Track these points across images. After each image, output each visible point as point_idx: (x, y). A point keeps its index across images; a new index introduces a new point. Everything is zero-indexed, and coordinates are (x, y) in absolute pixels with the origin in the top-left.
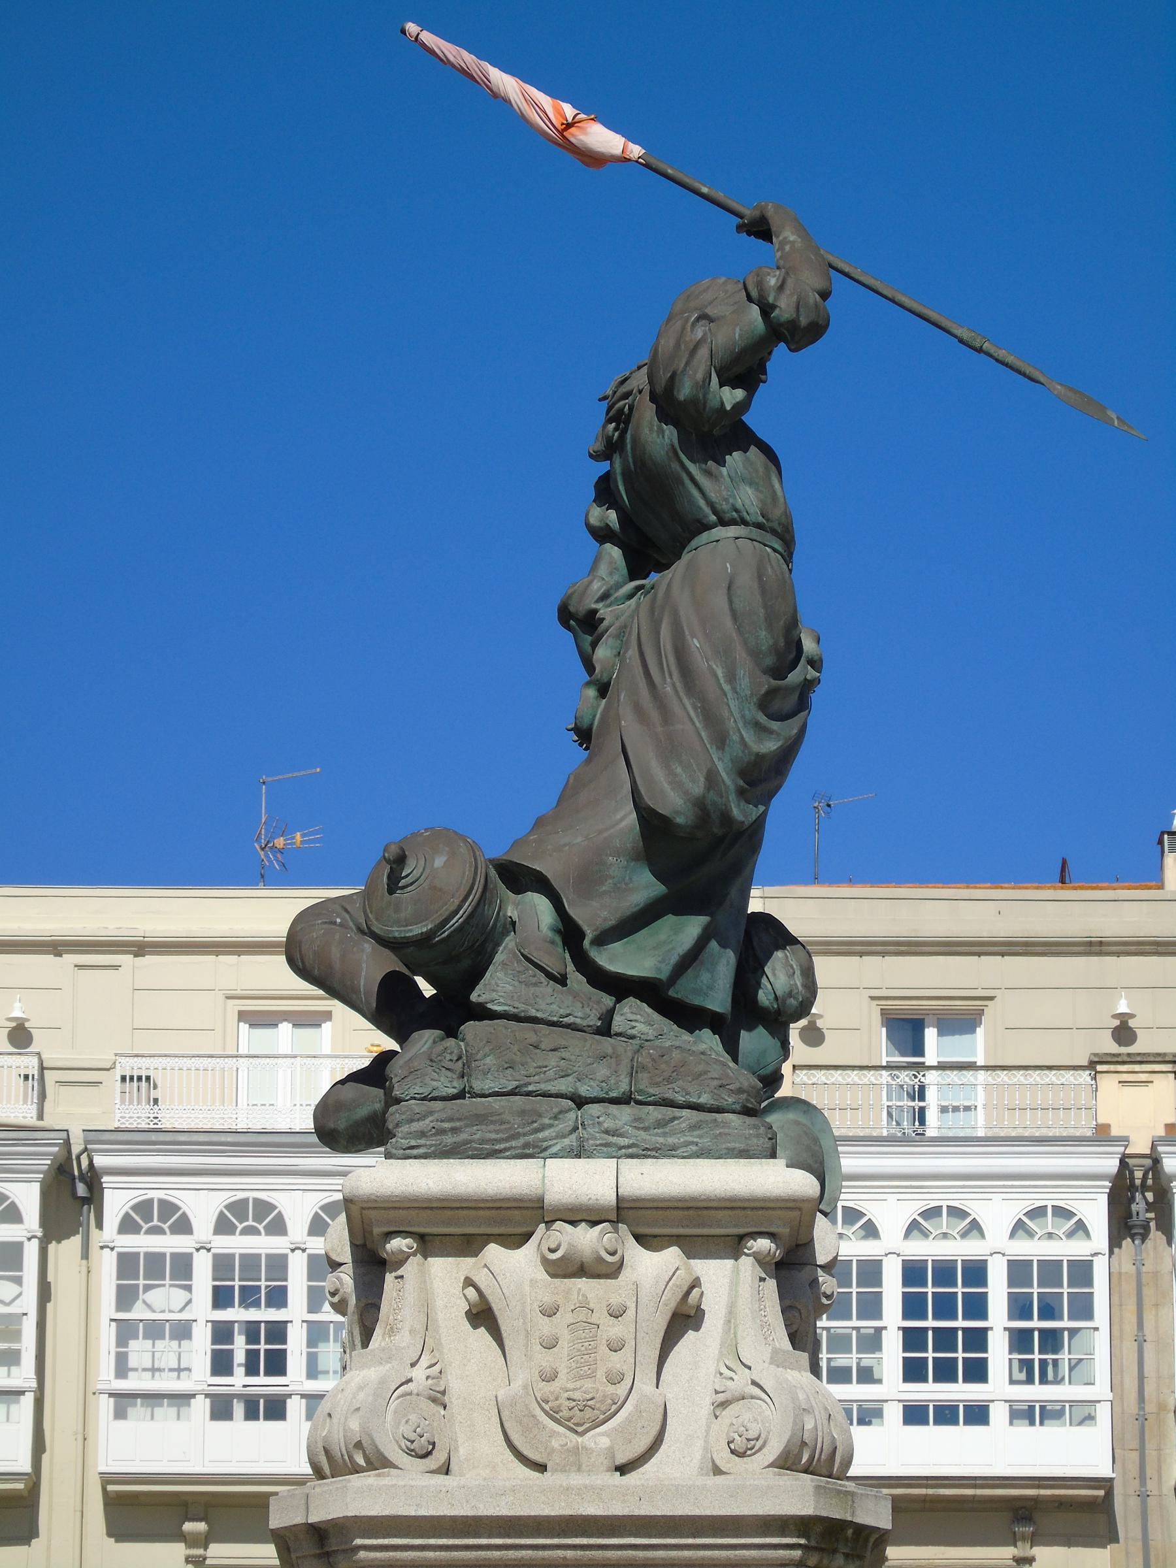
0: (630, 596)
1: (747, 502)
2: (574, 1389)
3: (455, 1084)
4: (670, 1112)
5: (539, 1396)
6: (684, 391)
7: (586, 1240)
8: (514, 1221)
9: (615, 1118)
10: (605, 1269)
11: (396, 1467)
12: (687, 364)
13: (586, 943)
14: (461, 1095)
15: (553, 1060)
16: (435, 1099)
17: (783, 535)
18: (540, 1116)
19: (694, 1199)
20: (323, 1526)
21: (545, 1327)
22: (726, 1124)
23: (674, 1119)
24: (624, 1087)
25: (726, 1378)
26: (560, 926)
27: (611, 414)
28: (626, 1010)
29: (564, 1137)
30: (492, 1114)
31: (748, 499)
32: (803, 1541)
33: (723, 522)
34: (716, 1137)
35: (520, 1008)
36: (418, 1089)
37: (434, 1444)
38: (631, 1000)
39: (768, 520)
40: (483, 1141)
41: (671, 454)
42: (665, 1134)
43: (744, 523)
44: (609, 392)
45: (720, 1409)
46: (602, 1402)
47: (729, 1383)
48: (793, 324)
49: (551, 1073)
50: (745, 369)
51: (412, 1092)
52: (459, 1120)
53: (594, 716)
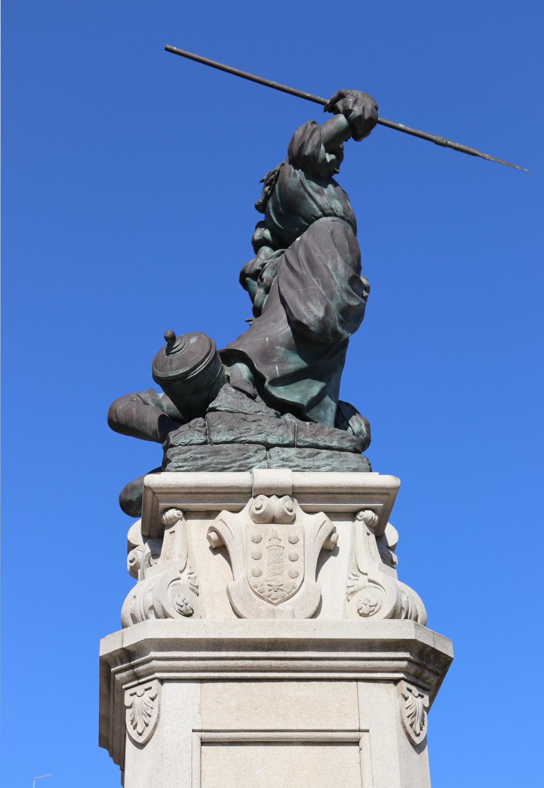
0: (278, 256)
1: (337, 206)
3: (202, 437)
4: (316, 450)
5: (251, 584)
6: (308, 150)
7: (277, 505)
9: (287, 452)
12: (310, 137)
13: (266, 384)
14: (205, 443)
15: (253, 426)
16: (192, 445)
18: (248, 451)
19: (333, 488)
20: (132, 649)
23: (319, 453)
24: (291, 438)
25: (353, 580)
26: (253, 378)
29: (260, 461)
30: (222, 451)
31: (337, 205)
32: (407, 655)
33: (325, 215)
34: (341, 462)
36: (182, 440)
37: (193, 610)
40: (218, 463)
41: (300, 185)
42: (314, 461)
43: (335, 215)
46: (287, 587)
47: (356, 582)
48: (361, 117)
51: (179, 442)
52: (205, 453)
53: (263, 301)
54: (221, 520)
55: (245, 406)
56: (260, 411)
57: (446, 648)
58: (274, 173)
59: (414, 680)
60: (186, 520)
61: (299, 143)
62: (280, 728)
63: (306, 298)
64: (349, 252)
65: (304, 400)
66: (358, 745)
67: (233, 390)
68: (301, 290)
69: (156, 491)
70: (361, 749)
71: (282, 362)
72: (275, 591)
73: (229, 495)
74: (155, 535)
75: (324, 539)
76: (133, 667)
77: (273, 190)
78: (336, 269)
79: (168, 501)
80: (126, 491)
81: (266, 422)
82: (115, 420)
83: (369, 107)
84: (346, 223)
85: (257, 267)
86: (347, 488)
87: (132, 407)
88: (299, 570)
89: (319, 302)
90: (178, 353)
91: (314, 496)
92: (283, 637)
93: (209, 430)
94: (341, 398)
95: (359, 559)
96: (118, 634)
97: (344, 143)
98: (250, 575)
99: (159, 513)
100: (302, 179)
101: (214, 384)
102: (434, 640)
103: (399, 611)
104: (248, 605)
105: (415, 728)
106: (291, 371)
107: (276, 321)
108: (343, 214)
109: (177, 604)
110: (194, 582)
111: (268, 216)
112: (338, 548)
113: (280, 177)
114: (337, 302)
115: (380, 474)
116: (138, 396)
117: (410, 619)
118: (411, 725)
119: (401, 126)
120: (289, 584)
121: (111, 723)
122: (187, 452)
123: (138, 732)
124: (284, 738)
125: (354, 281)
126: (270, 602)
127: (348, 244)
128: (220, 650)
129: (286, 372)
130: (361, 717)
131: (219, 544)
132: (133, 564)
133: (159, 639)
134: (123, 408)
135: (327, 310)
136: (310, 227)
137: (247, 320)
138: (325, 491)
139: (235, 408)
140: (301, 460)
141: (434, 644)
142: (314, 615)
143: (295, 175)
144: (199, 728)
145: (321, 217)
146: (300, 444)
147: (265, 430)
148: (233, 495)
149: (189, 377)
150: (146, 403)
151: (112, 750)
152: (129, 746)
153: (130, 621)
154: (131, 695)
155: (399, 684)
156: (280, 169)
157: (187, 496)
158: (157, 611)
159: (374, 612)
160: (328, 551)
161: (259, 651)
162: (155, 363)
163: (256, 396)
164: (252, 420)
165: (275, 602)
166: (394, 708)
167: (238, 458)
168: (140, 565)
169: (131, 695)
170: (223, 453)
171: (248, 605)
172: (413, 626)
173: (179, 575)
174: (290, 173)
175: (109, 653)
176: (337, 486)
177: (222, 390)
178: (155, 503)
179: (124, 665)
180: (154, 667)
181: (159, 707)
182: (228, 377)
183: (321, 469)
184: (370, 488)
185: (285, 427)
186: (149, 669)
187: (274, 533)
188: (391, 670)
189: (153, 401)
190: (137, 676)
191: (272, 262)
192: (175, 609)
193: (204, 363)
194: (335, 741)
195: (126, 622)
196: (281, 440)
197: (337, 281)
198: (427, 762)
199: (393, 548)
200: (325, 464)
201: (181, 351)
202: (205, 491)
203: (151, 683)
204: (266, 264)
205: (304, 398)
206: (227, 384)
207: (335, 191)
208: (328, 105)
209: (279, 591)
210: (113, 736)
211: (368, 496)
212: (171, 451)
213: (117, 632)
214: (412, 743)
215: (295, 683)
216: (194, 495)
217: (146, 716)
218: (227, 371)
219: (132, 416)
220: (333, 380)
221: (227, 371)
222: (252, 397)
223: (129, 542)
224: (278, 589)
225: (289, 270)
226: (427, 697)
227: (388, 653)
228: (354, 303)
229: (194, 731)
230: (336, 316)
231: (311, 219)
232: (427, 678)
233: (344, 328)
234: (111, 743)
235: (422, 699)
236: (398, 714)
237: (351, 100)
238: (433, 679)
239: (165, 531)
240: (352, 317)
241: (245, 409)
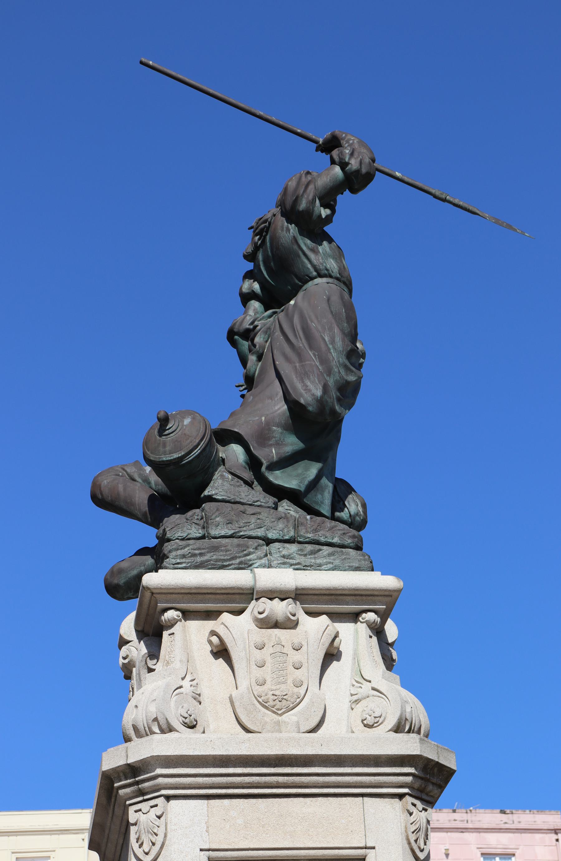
0: (270, 316)
3: (200, 531)
4: (317, 547)
5: (255, 693)
6: (303, 205)
7: (280, 608)
8: (238, 599)
10: (290, 624)
11: (178, 731)
13: (263, 469)
14: (203, 537)
15: (253, 519)
16: (189, 539)
17: (346, 283)
18: (248, 547)
19: (336, 589)
21: (258, 655)
22: (348, 554)
23: (320, 550)
24: (292, 533)
25: (357, 687)
26: (249, 461)
27: (257, 231)
28: (284, 504)
29: (261, 558)
30: (221, 546)
31: (332, 265)
32: (412, 770)
33: (320, 276)
35: (232, 497)
36: (180, 534)
37: (196, 721)
38: (286, 501)
39: (342, 276)
40: (217, 561)
41: (293, 241)
42: (315, 558)
43: (331, 276)
45: (355, 704)
46: (292, 697)
47: (359, 689)
48: (358, 172)
50: (328, 198)
52: (203, 549)
53: (256, 370)
55: (243, 495)
57: (449, 761)
58: (265, 221)
59: (418, 794)
62: (287, 846)
63: (303, 375)
65: (301, 485)
67: (230, 477)
68: (297, 365)
69: (154, 591)
72: (280, 701)
74: (152, 632)
75: (327, 645)
76: (138, 783)
77: (264, 242)
78: (333, 342)
79: (167, 602)
82: (100, 496)
83: (367, 160)
86: (350, 590)
87: (118, 483)
88: (303, 679)
89: (317, 380)
90: (171, 435)
91: (316, 597)
92: (290, 753)
93: (207, 523)
94: (338, 475)
95: (361, 664)
98: (254, 684)
99: (157, 612)
100: (295, 234)
101: (209, 468)
104: (252, 716)
105: (420, 844)
109: (181, 716)
110: (196, 690)
111: (257, 266)
112: (341, 652)
113: (272, 229)
114: (335, 379)
115: (382, 574)
116: (124, 469)
119: (398, 174)
120: (293, 694)
121: (107, 831)
122: (185, 547)
127: (345, 312)
128: (226, 766)
129: (283, 456)
130: (368, 834)
132: (126, 661)
133: (165, 756)
135: (325, 388)
136: (304, 288)
137: (237, 385)
138: (327, 592)
139: (232, 497)
140: (303, 557)
143: (288, 230)
144: (206, 847)
145: (315, 278)
146: (300, 540)
148: (235, 596)
149: (184, 462)
150: (134, 480)
151: (105, 854)
153: (132, 733)
154: (136, 811)
157: (186, 597)
158: (161, 724)
159: (378, 724)
160: (331, 655)
161: (266, 767)
162: (146, 443)
163: (253, 483)
164: (251, 513)
165: (280, 712)
166: (399, 824)
167: (237, 555)
169: (136, 811)
170: (223, 548)
171: (252, 716)
175: (113, 768)
176: (340, 588)
178: (153, 603)
179: (129, 781)
180: (160, 784)
182: (223, 460)
183: (323, 567)
184: (373, 590)
186: (155, 786)
189: (140, 475)
190: (142, 793)
192: (179, 721)
193: (199, 447)
195: (128, 733)
196: (281, 536)
199: (392, 645)
200: (326, 562)
201: (175, 433)
202: (206, 591)
203: (156, 800)
204: (257, 326)
205: (301, 482)
206: (222, 466)
207: (330, 248)
208: (320, 145)
209: (284, 701)
215: (301, 799)
217: (152, 835)
220: (330, 459)
222: (249, 484)
223: (121, 637)
224: (283, 699)
225: (284, 340)
227: (394, 768)
228: (352, 378)
229: (201, 850)
230: (334, 393)
231: (306, 279)
233: (341, 406)
235: (426, 813)
236: (403, 830)
237: (347, 151)
240: (348, 392)
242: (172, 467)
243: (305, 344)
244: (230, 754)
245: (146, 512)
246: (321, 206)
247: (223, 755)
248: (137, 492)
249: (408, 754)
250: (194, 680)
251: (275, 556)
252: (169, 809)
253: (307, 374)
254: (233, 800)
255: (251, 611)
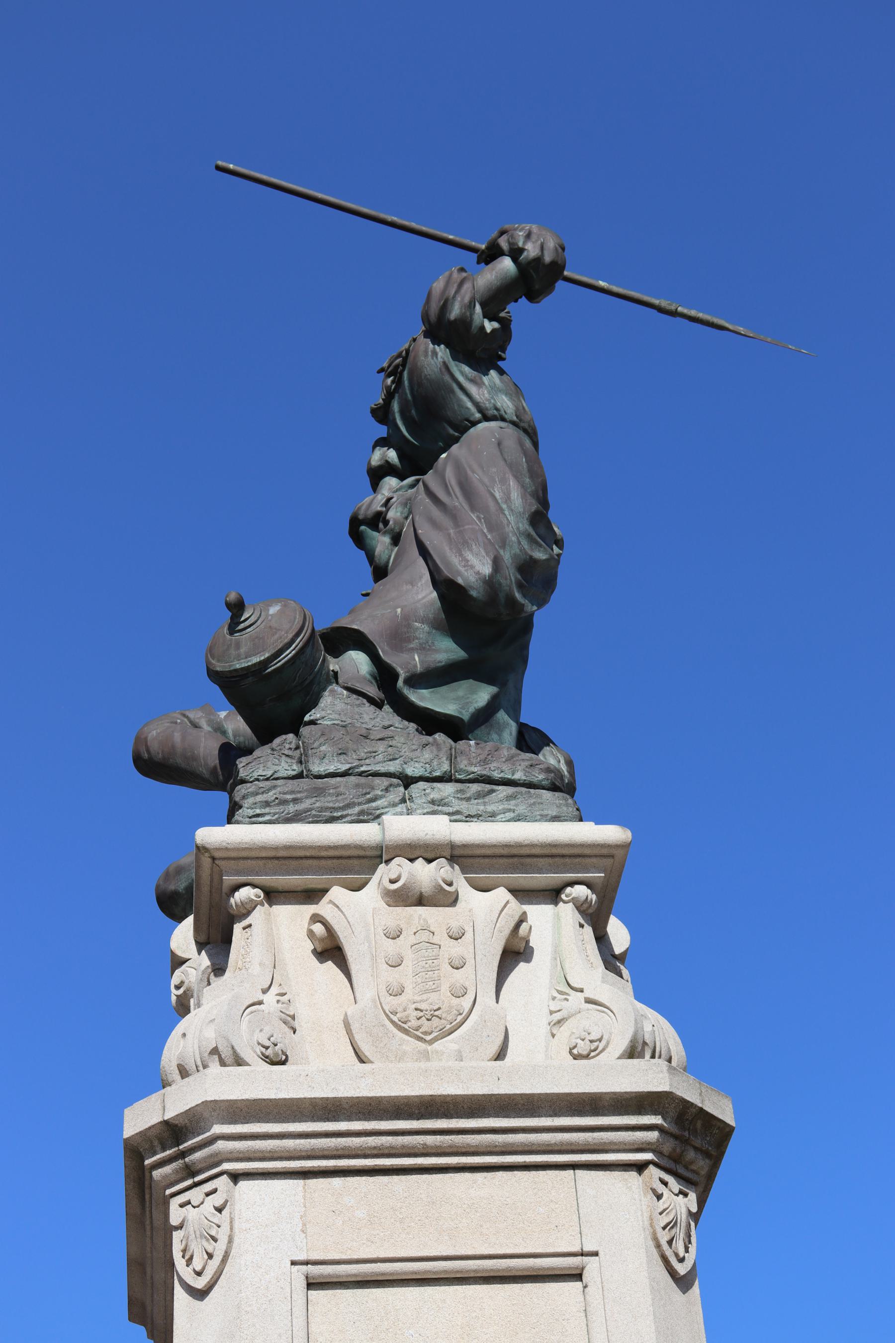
0: (412, 486)
2: (421, 1001)
3: (295, 767)
4: (488, 787)
6: (455, 312)
7: (425, 874)
8: (357, 864)
12: (457, 292)
13: (400, 683)
14: (300, 776)
15: (381, 747)
18: (373, 789)
19: (520, 845)
20: (180, 1122)
23: (493, 791)
24: (446, 767)
25: (560, 1000)
29: (394, 805)
31: (506, 403)
32: (657, 1120)
33: (486, 418)
34: (531, 805)
36: (261, 772)
37: (287, 1056)
40: (322, 810)
41: (444, 370)
42: (485, 804)
43: (503, 419)
44: (385, 365)
46: (449, 1012)
48: (538, 260)
49: (380, 757)
51: (255, 775)
52: (300, 792)
53: (390, 557)
54: (331, 902)
55: (366, 718)
56: (392, 726)
57: (723, 1109)
58: (399, 355)
60: (271, 906)
61: (439, 301)
62: (445, 1254)
63: (461, 544)
64: (527, 475)
65: (464, 711)
66: (582, 1281)
67: (345, 692)
68: (452, 531)
69: (217, 855)
70: (585, 1287)
71: (424, 648)
73: (344, 862)
74: (217, 940)
75: (507, 932)
76: (183, 1155)
77: (399, 382)
78: (508, 499)
79: (238, 873)
80: (167, 876)
81: (402, 740)
82: (146, 756)
83: (551, 244)
84: (522, 432)
85: (378, 507)
86: (544, 845)
87: (173, 732)
88: (467, 984)
91: (487, 860)
93: (306, 756)
94: (523, 720)
95: (567, 966)
96: (154, 1099)
97: (513, 304)
99: (224, 894)
100: (446, 359)
101: (312, 683)
102: (700, 1094)
103: (639, 1049)
104: (382, 1045)
106: (440, 664)
107: (412, 583)
108: (515, 418)
109: (259, 1044)
110: (287, 1009)
114: (513, 552)
116: (184, 715)
117: (660, 1057)
118: (670, 1243)
119: (602, 284)
120: (451, 1007)
121: (148, 1270)
122: (269, 790)
123: (194, 1270)
124: (452, 1272)
125: (538, 518)
126: (419, 1039)
127: (526, 461)
128: (335, 1119)
129: (433, 666)
131: (329, 945)
132: (181, 991)
133: (227, 1101)
134: (158, 734)
135: (497, 563)
136: (462, 439)
137: (364, 592)
140: (464, 802)
141: (702, 1102)
142: (501, 1055)
143: (435, 353)
144: (302, 1257)
146: (460, 777)
147: (401, 754)
148: (351, 861)
149: (269, 670)
150: (195, 726)
152: (179, 1293)
153: (176, 1075)
155: (646, 1172)
156: (410, 346)
157: (270, 864)
158: (223, 1056)
159: (597, 1052)
160: (515, 953)
162: (210, 650)
164: (378, 737)
165: (428, 1038)
167: (356, 801)
168: (192, 991)
170: (331, 791)
171: (382, 1045)
172: (665, 1068)
173: (261, 997)
174: (426, 352)
175: (140, 1132)
176: (527, 842)
177: (326, 693)
179: (168, 1152)
181: (231, 1222)
182: (336, 674)
183: (498, 817)
184: (582, 845)
185: (434, 748)
186: (211, 1156)
187: (422, 921)
188: (632, 1147)
189: (210, 722)
191: (402, 495)
192: (255, 1052)
193: (294, 646)
194: (541, 1273)
196: (429, 770)
197: (511, 518)
198: (698, 1308)
199: (621, 958)
200: (504, 809)
201: (254, 626)
204: (392, 498)
205: (463, 708)
207: (501, 380)
208: (483, 251)
210: (152, 1296)
211: (577, 860)
212: (241, 790)
213: (154, 1095)
214: (672, 1273)
215: (467, 1175)
216: (283, 862)
217: (207, 1240)
218: (333, 664)
219: (173, 747)
221: (333, 664)
222: (379, 705)
223: (173, 954)
224: (433, 1016)
226: (693, 1196)
227: (625, 1117)
229: (293, 1263)
230: (510, 576)
231: (464, 426)
232: (691, 1163)
233: (524, 596)
234: (149, 1308)
235: (686, 1199)
236: (647, 1223)
238: (702, 1164)
239: (235, 926)
240: (538, 578)
241: (366, 723)
242: (250, 679)
243: (464, 504)
244: (340, 1095)
245: (215, 768)
246: (484, 317)
247: (327, 1099)
248: (203, 739)
249: (649, 1090)
250: (285, 994)
251: (419, 802)
252: (237, 1195)
253: (467, 543)
254: (348, 1179)
255: (378, 881)
